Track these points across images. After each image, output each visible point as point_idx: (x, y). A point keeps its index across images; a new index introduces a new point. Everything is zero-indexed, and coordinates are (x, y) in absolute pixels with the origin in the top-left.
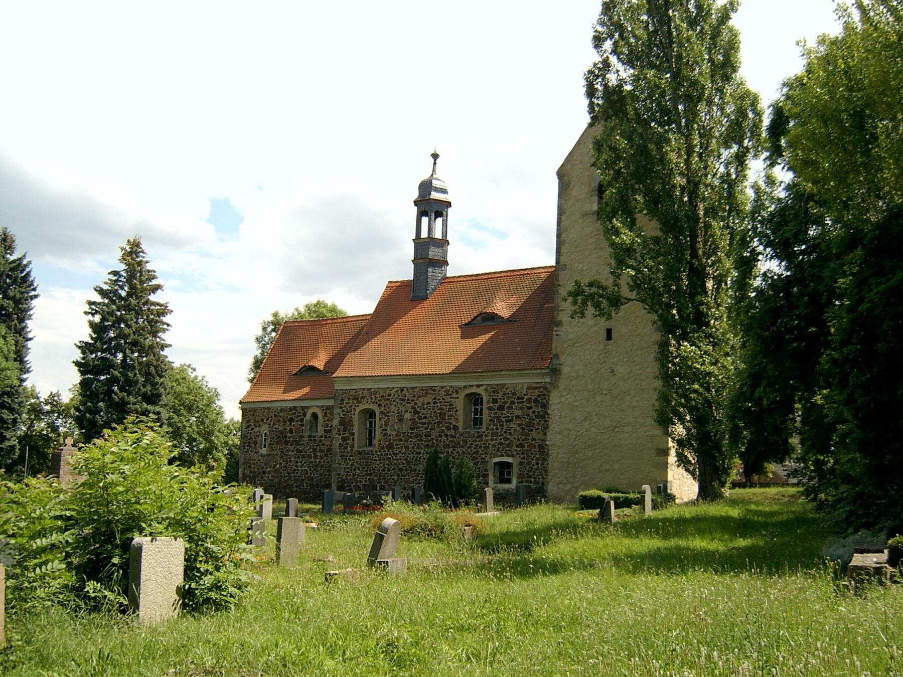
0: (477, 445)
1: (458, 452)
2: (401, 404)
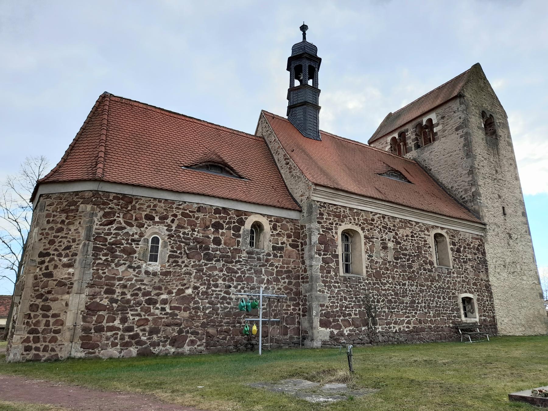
0: (448, 281)
1: (435, 287)
2: (384, 231)
